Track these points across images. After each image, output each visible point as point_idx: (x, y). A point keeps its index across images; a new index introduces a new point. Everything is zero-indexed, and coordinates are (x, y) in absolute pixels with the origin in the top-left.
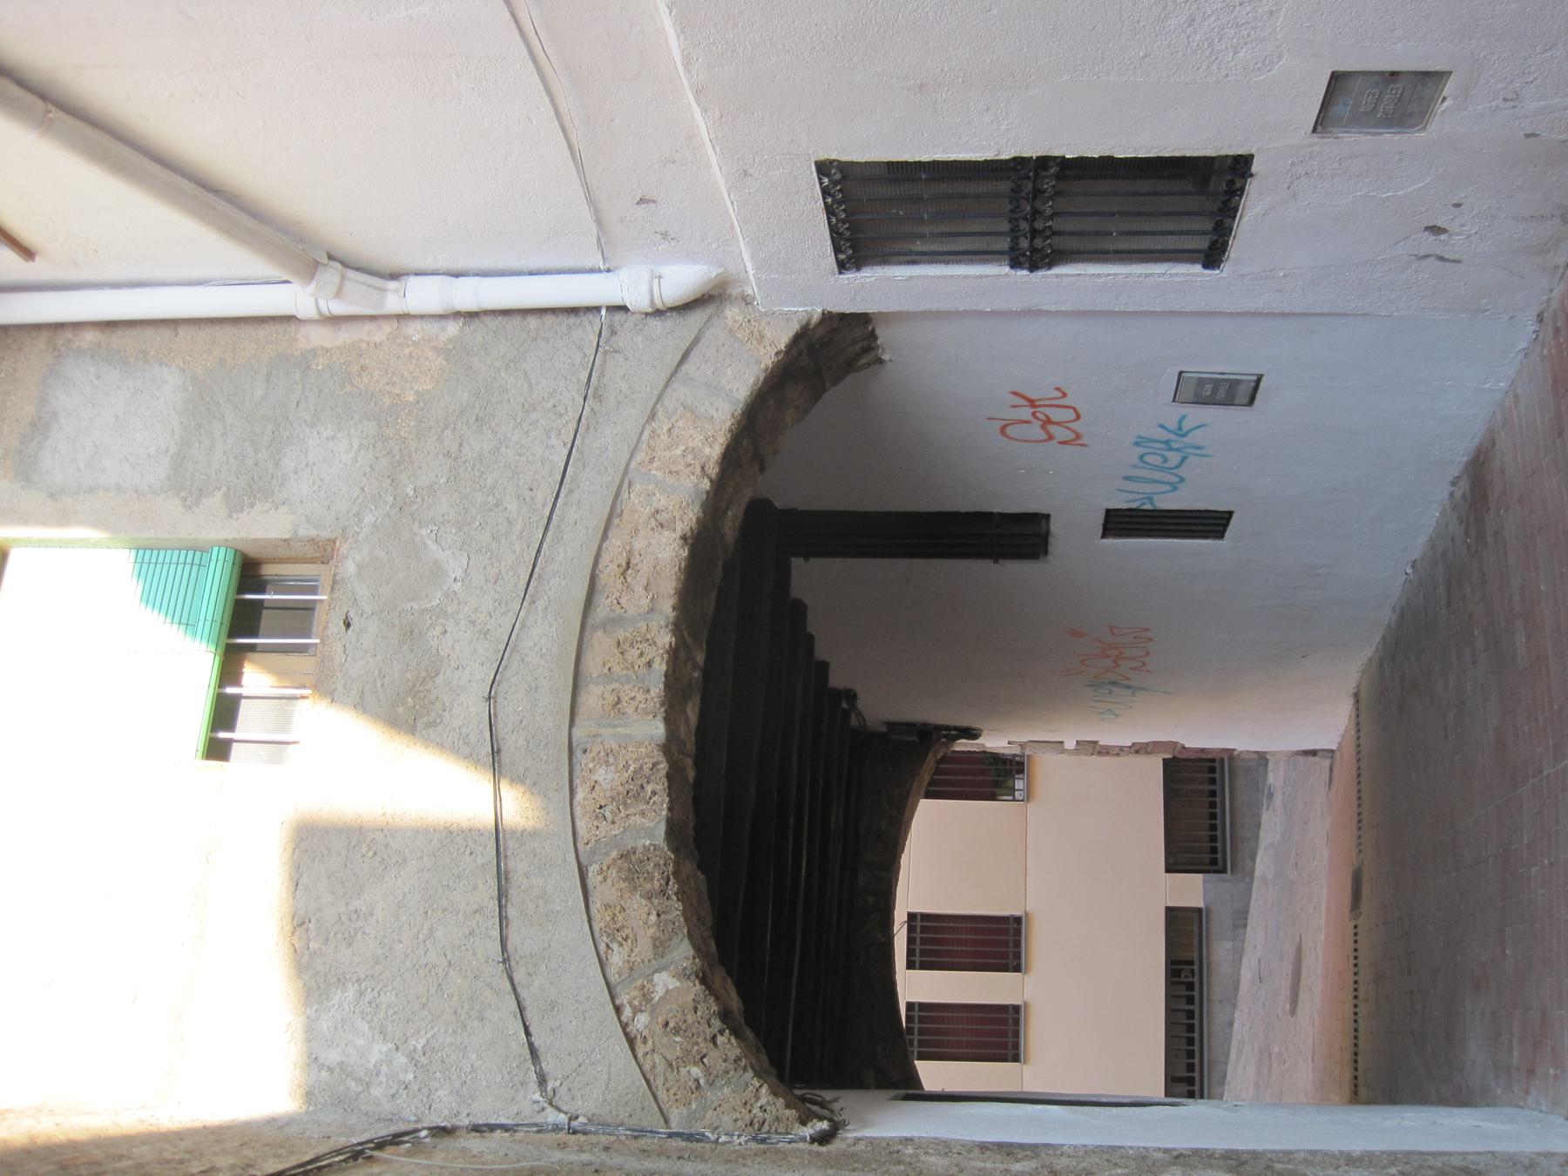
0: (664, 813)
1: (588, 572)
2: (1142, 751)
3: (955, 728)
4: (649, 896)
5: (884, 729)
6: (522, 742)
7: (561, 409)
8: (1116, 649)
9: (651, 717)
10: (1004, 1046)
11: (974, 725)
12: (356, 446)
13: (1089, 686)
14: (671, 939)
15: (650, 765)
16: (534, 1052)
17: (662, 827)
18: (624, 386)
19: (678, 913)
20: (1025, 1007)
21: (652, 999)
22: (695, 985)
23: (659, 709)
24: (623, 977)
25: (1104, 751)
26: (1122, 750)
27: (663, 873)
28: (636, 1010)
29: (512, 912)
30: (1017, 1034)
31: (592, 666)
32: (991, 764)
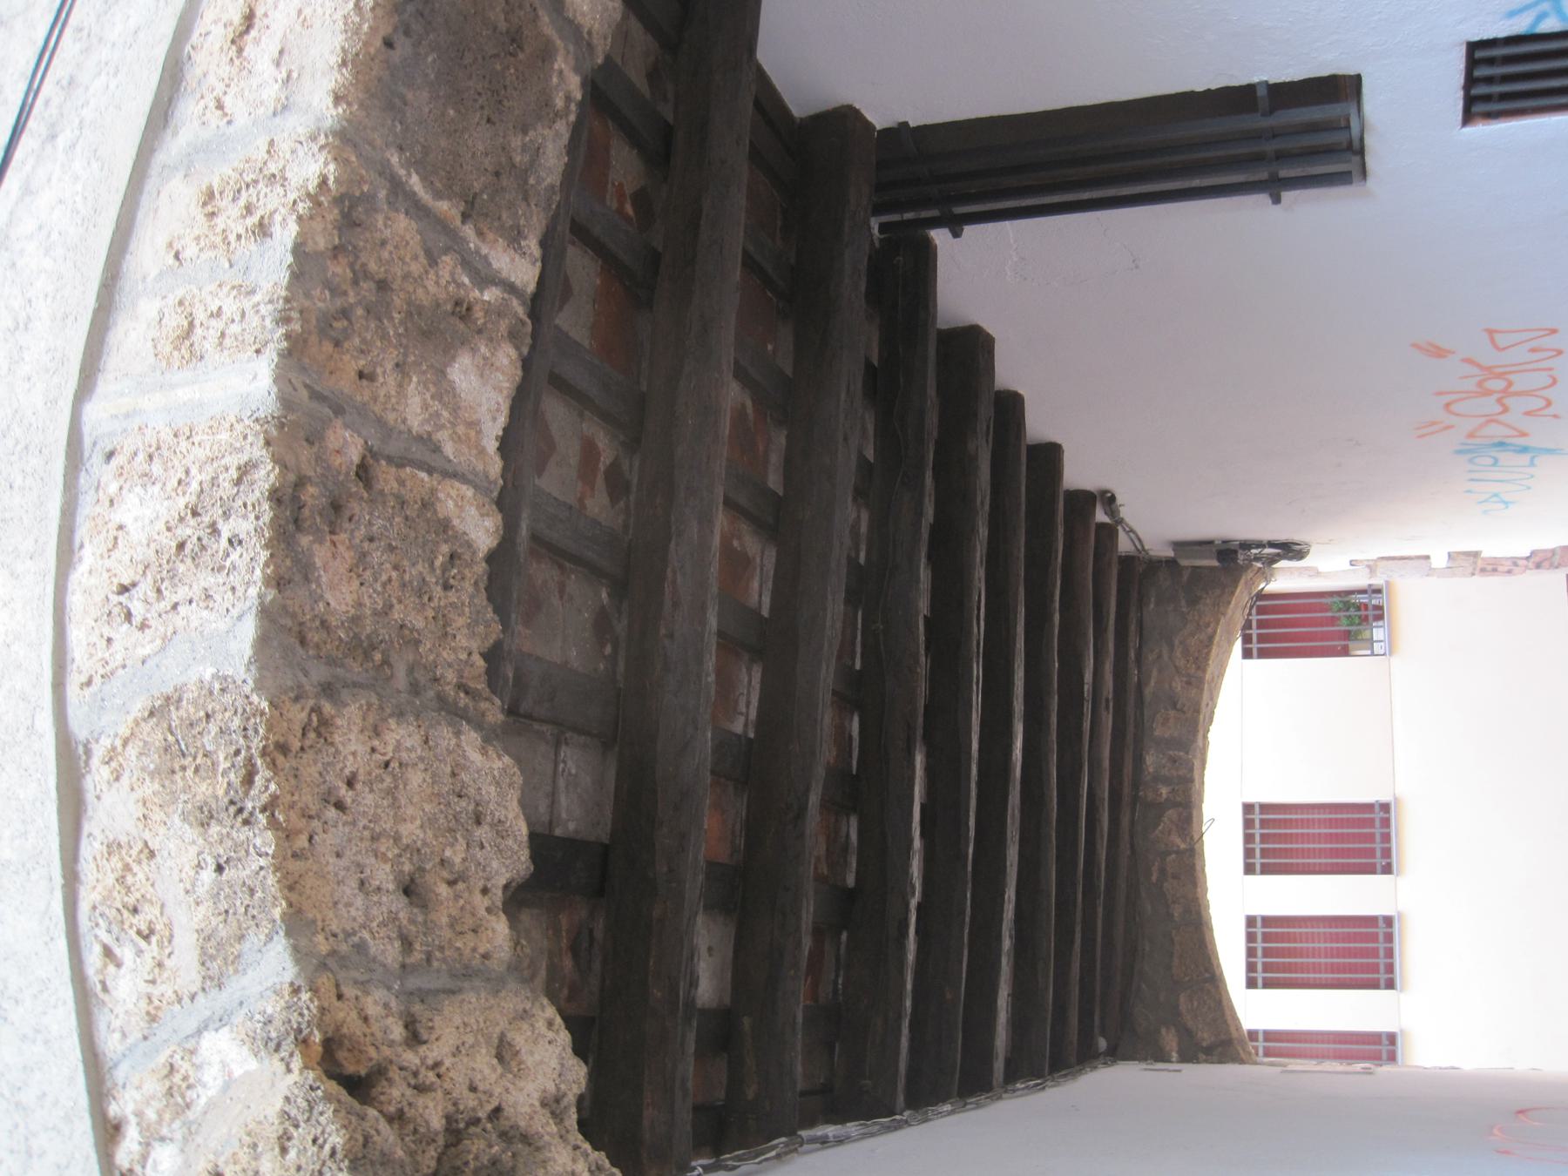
0: (253, 592)
2: (1546, 564)
3: (1272, 544)
4: (205, 817)
5: (1171, 553)
8: (1500, 376)
9: (250, 352)
10: (1374, 968)
11: (1296, 538)
13: (1459, 452)
14: (241, 938)
15: (234, 474)
17: (248, 629)
19: (263, 862)
20: (1399, 917)
21: (188, 1106)
22: (289, 1070)
23: (272, 332)
24: (130, 1040)
25: (1489, 568)
26: (1515, 564)
27: (237, 752)
31: (147, 256)
32: (1340, 610)
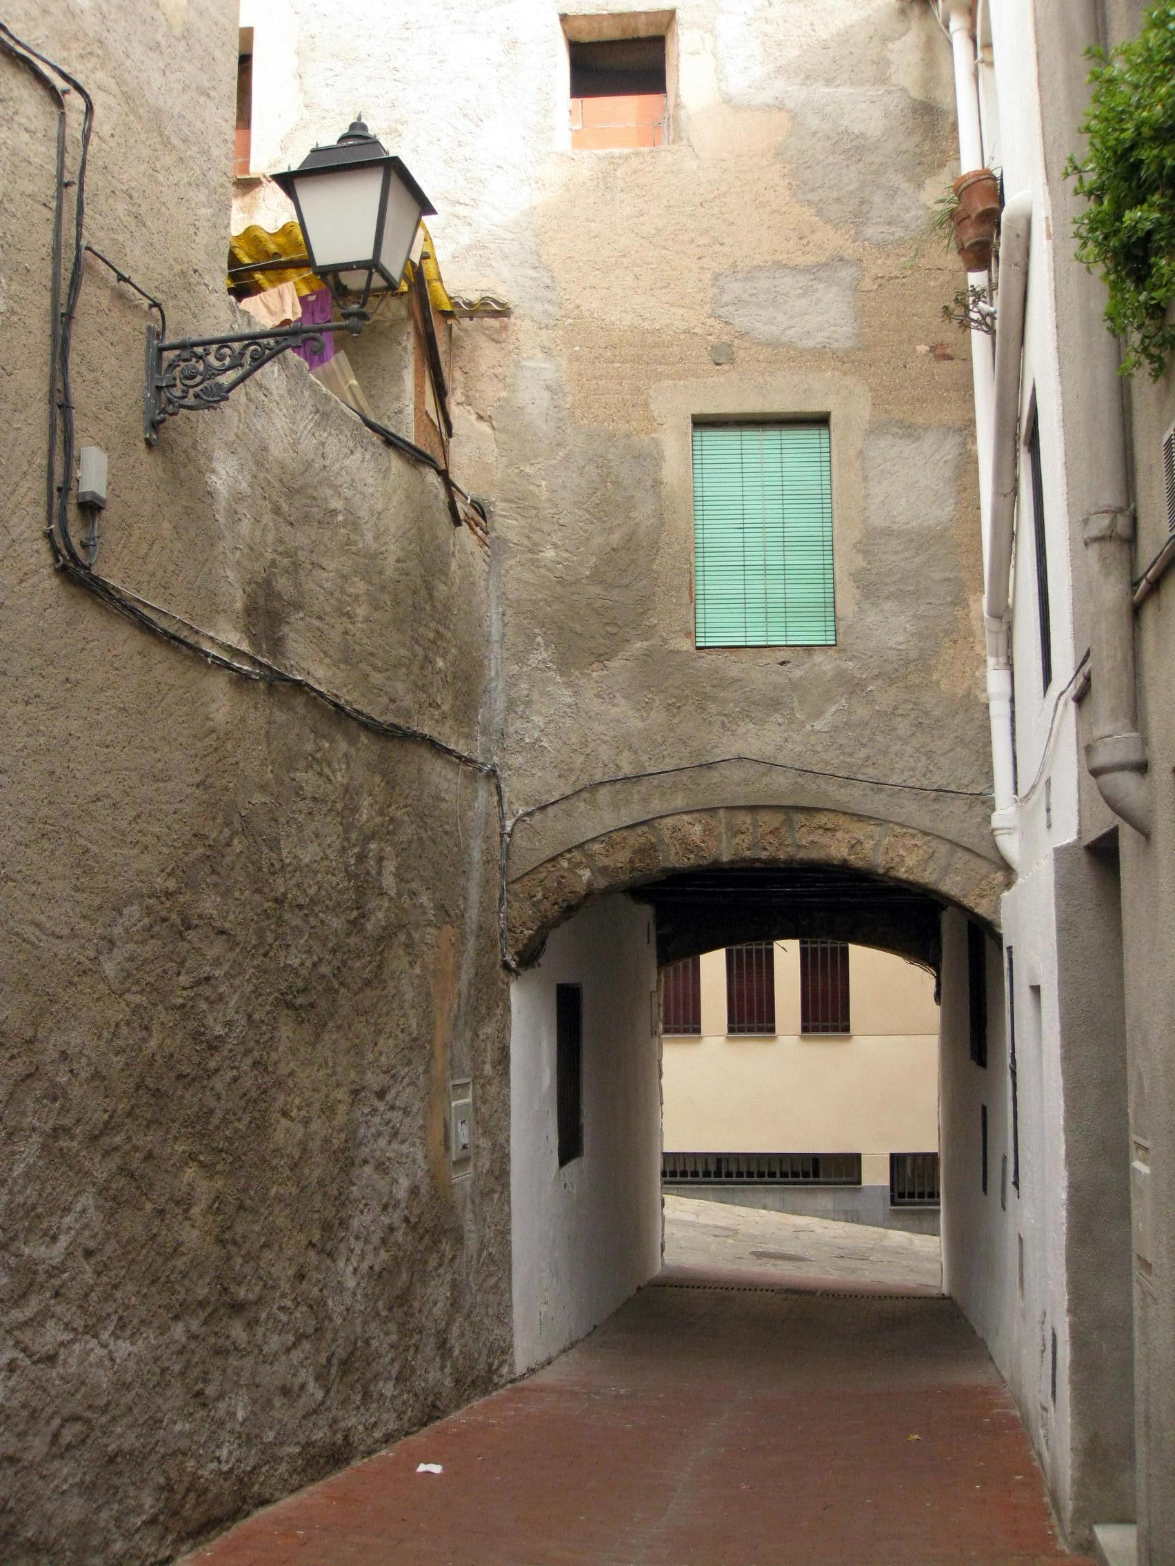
1: (820, 805)
4: (631, 861)
6: (714, 780)
7: (929, 775)
12: (902, 647)
16: (543, 808)
18: (946, 813)
28: (569, 860)
29: (618, 786)
30: (751, 1030)
